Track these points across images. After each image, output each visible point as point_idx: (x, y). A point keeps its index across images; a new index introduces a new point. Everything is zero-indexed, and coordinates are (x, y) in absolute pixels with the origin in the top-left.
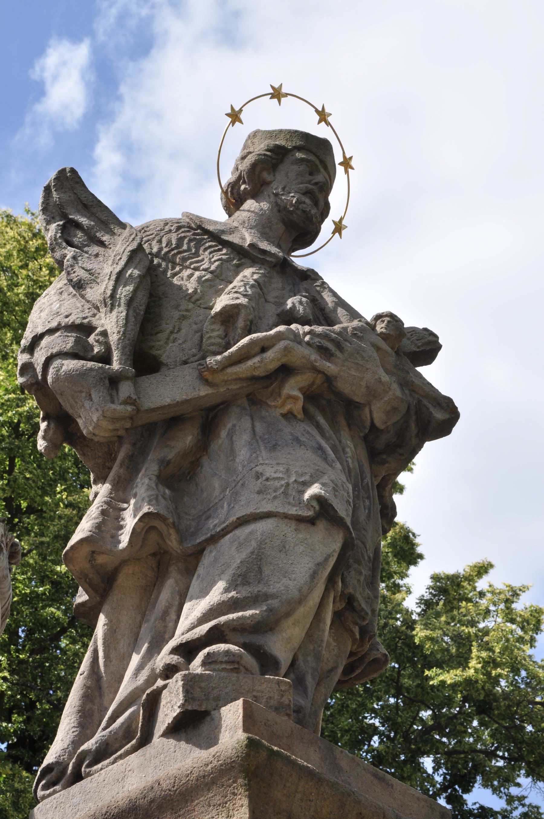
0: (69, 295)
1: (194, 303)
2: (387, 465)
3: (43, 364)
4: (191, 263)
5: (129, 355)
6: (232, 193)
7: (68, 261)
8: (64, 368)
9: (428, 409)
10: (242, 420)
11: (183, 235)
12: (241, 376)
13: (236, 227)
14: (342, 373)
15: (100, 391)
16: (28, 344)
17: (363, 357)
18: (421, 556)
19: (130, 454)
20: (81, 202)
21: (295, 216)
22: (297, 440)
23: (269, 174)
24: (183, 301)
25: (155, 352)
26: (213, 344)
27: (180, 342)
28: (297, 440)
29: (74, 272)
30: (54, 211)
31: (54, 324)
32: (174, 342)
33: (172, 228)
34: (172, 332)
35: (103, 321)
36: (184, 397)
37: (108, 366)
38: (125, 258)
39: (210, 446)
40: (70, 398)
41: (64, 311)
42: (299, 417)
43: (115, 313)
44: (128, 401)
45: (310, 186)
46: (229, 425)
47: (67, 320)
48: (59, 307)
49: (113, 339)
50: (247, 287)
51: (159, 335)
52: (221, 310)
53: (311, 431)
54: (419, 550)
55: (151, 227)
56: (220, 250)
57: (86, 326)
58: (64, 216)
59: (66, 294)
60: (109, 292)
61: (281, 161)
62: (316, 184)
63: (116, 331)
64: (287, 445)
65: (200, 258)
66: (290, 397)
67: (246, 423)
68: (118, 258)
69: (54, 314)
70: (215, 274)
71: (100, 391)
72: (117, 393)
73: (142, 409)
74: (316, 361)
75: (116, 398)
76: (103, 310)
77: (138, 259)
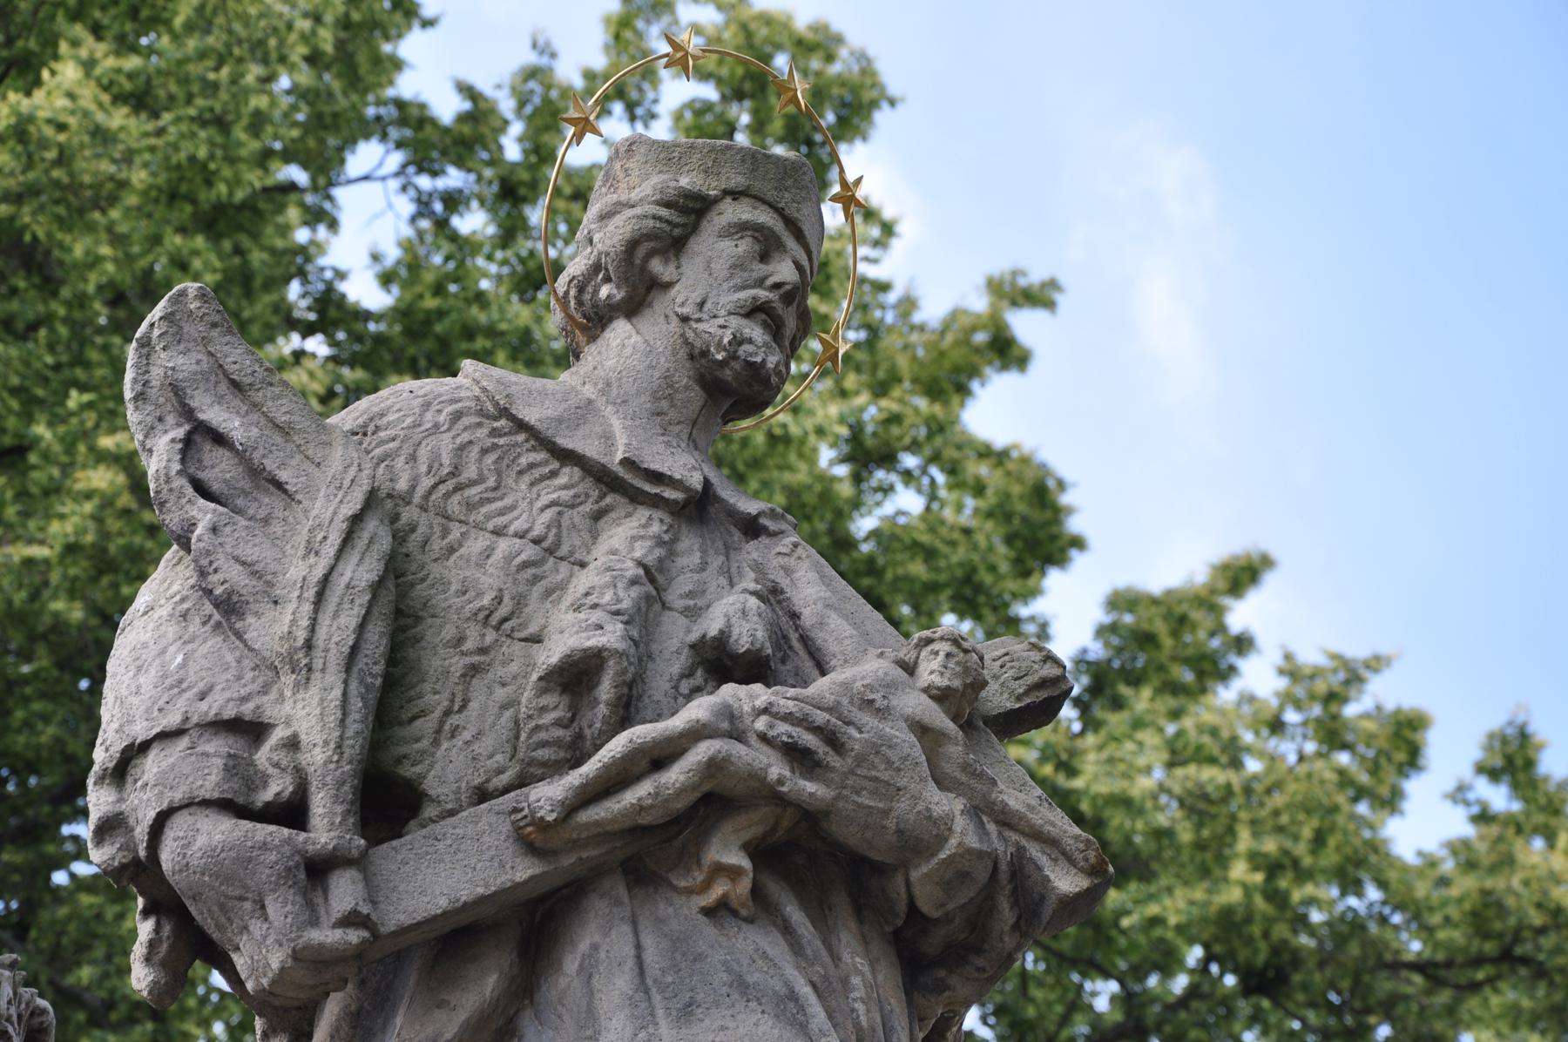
0: (204, 623)
1: (497, 628)
2: (947, 993)
3: (152, 827)
4: (488, 517)
5: (352, 803)
6: (580, 303)
7: (199, 540)
8: (201, 841)
9: (1039, 869)
10: (614, 932)
11: (466, 437)
12: (609, 828)
13: (590, 402)
14: (841, 804)
15: (285, 903)
16: (111, 765)
17: (889, 763)
18: (1078, 543)
19: (353, 1008)
20: (226, 374)
21: (728, 372)
22: (742, 986)
23: (667, 261)
24: (471, 624)
25: (408, 771)
26: (543, 744)
27: (467, 735)
28: (742, 986)
29: (216, 571)
30: (162, 400)
31: (173, 719)
32: (453, 737)
33: (441, 418)
34: (447, 713)
35: (287, 707)
36: (480, 890)
37: (302, 836)
38: (335, 539)
39: (539, 987)
40: (215, 908)
41: (196, 678)
42: (744, 913)
43: (314, 691)
44: (351, 920)
45: (763, 294)
46: (584, 946)
47: (203, 706)
48: (184, 665)
49: (316, 757)
50: (620, 585)
51: (418, 723)
52: (561, 661)
53: (771, 952)
54: (1074, 525)
55: (391, 417)
56: (554, 474)
57: (250, 723)
58: (188, 413)
59: (197, 620)
60: (301, 635)
61: (693, 229)
62: (777, 286)
63: (319, 739)
64: (717, 1004)
65: (508, 501)
66: (720, 870)
67: (619, 943)
68: (319, 537)
69: (172, 687)
70: (545, 544)
71: (285, 903)
72: (326, 898)
73: (383, 930)
74: (780, 782)
75: (322, 911)
76: (288, 679)
77: (366, 536)
